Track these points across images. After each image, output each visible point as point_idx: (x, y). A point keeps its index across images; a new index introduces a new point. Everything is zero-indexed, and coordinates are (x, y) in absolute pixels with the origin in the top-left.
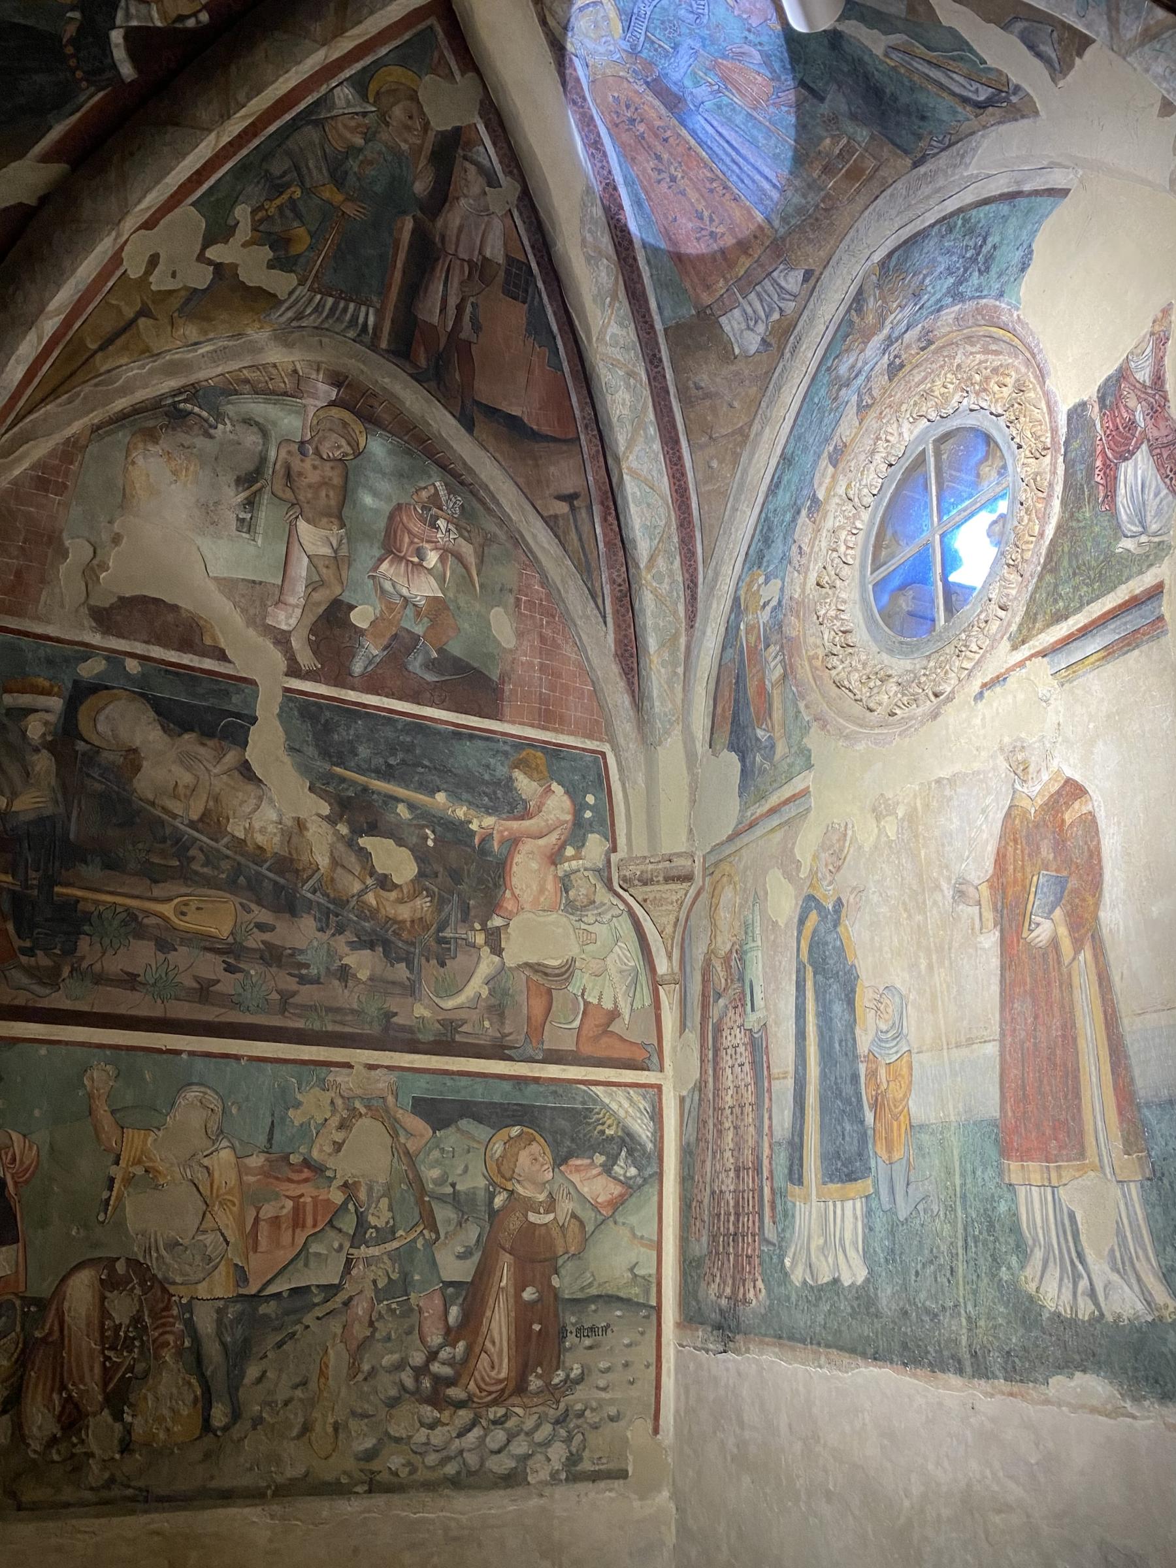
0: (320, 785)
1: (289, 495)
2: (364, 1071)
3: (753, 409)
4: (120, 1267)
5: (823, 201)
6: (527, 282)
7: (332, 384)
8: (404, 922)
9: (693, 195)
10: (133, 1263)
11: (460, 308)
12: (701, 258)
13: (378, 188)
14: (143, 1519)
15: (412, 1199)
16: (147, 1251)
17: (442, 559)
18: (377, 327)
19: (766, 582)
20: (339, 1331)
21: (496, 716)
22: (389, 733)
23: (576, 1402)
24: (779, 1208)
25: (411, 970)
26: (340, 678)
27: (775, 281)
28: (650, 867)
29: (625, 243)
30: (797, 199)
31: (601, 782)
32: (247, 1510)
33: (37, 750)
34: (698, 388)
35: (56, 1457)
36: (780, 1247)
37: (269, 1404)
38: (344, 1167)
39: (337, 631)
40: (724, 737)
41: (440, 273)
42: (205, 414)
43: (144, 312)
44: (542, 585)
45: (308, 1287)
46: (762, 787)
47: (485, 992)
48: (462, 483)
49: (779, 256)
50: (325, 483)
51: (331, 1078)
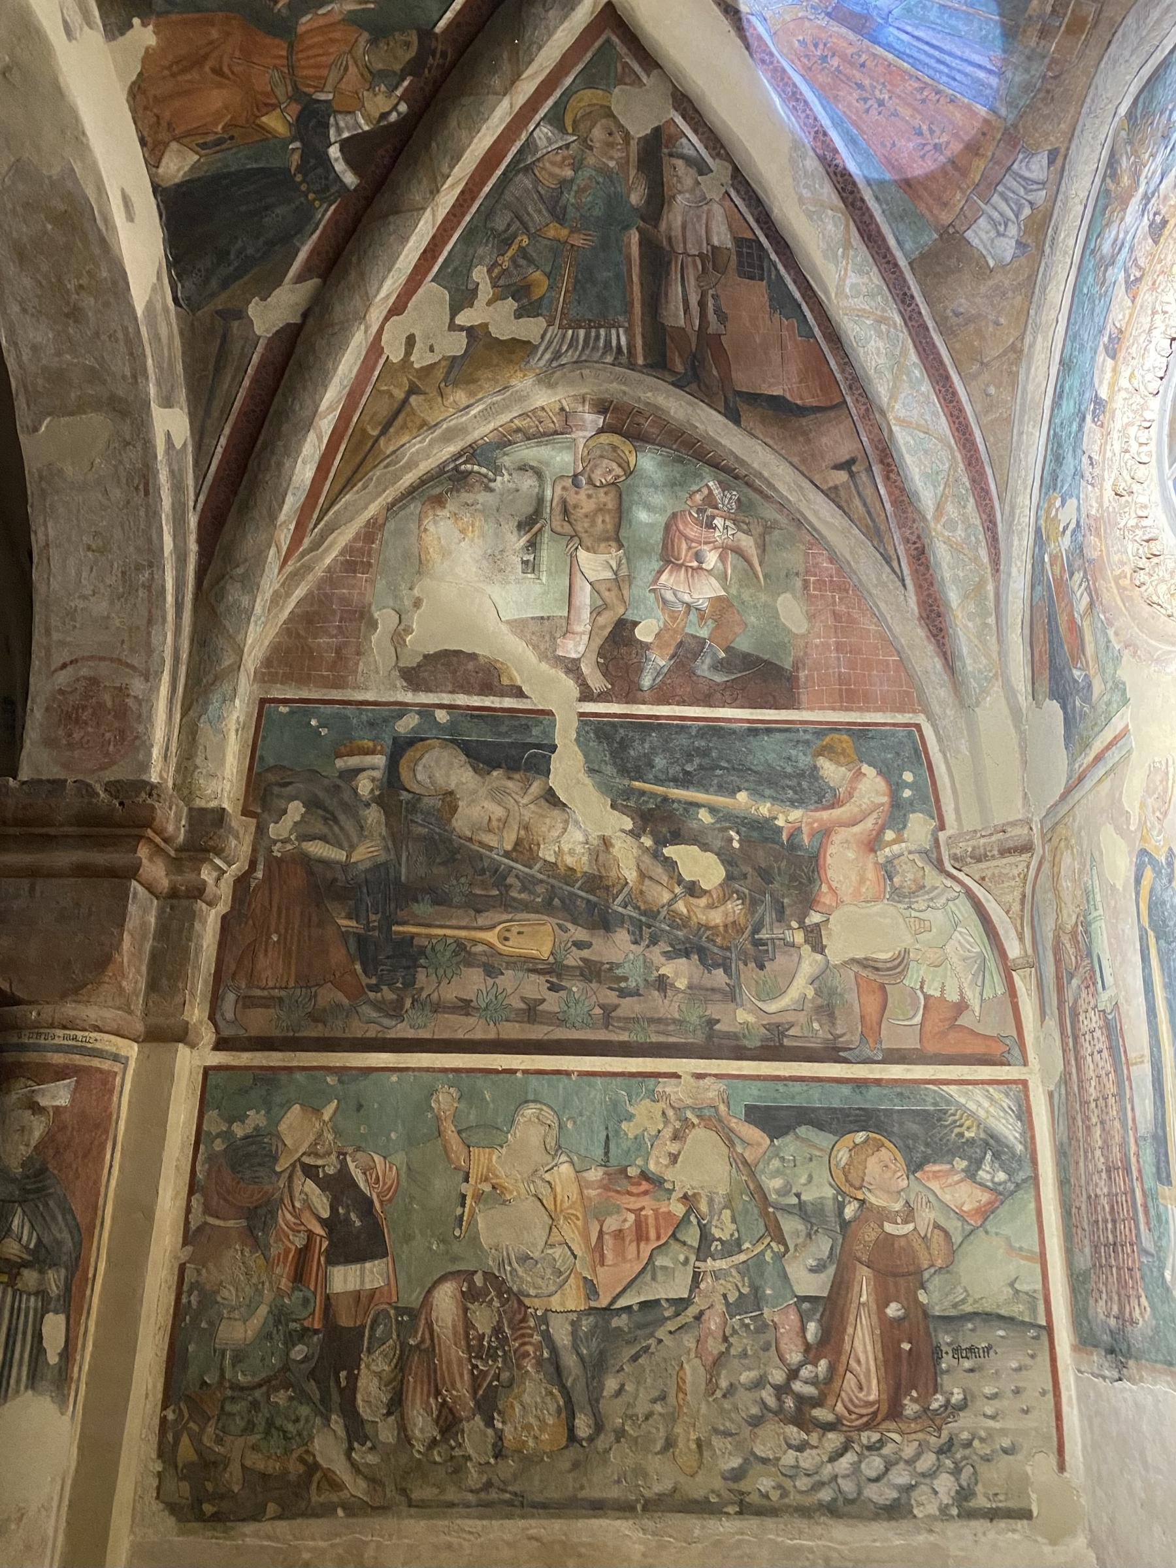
0: (621, 800)
1: (567, 528)
2: (692, 1080)
3: (1023, 320)
4: (478, 1280)
5: (1049, 68)
6: (760, 259)
7: (599, 413)
8: (717, 927)
9: (906, 112)
10: (488, 1276)
11: (702, 304)
12: (931, 177)
13: (597, 212)
14: (521, 1523)
15: (756, 1211)
16: (501, 1265)
17: (722, 558)
18: (631, 346)
19: (1063, 504)
20: (693, 1346)
21: (791, 703)
22: (683, 740)
23: (962, 1430)
24: (1152, 1212)
25: (730, 976)
26: (630, 694)
27: (1017, 174)
28: (982, 841)
29: (849, 187)
30: (1019, 78)
31: (919, 756)
32: (618, 1523)
33: (368, 805)
34: (957, 315)
35: (438, 1459)
36: (1159, 1259)
37: (631, 1417)
38: (682, 1178)
39: (623, 650)
40: (1044, 686)
41: (675, 275)
42: (484, 470)
43: (413, 390)
44: (831, 561)
45: (657, 1301)
46: (1085, 734)
47: (810, 993)
48: (736, 477)
49: (1014, 147)
50: (601, 509)
51: (659, 1089)
